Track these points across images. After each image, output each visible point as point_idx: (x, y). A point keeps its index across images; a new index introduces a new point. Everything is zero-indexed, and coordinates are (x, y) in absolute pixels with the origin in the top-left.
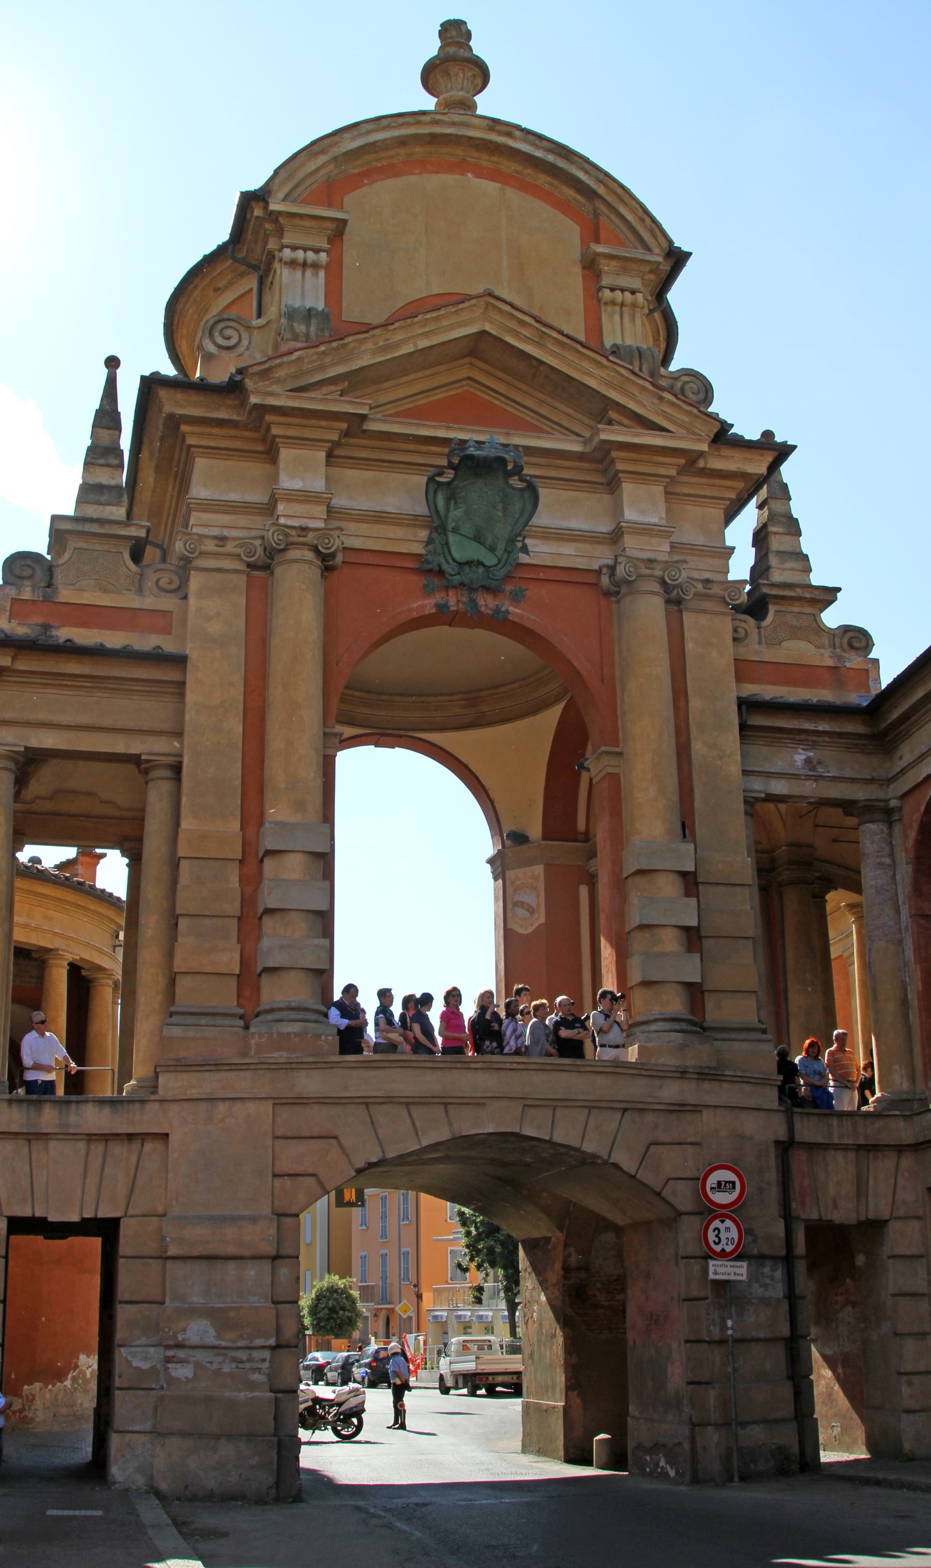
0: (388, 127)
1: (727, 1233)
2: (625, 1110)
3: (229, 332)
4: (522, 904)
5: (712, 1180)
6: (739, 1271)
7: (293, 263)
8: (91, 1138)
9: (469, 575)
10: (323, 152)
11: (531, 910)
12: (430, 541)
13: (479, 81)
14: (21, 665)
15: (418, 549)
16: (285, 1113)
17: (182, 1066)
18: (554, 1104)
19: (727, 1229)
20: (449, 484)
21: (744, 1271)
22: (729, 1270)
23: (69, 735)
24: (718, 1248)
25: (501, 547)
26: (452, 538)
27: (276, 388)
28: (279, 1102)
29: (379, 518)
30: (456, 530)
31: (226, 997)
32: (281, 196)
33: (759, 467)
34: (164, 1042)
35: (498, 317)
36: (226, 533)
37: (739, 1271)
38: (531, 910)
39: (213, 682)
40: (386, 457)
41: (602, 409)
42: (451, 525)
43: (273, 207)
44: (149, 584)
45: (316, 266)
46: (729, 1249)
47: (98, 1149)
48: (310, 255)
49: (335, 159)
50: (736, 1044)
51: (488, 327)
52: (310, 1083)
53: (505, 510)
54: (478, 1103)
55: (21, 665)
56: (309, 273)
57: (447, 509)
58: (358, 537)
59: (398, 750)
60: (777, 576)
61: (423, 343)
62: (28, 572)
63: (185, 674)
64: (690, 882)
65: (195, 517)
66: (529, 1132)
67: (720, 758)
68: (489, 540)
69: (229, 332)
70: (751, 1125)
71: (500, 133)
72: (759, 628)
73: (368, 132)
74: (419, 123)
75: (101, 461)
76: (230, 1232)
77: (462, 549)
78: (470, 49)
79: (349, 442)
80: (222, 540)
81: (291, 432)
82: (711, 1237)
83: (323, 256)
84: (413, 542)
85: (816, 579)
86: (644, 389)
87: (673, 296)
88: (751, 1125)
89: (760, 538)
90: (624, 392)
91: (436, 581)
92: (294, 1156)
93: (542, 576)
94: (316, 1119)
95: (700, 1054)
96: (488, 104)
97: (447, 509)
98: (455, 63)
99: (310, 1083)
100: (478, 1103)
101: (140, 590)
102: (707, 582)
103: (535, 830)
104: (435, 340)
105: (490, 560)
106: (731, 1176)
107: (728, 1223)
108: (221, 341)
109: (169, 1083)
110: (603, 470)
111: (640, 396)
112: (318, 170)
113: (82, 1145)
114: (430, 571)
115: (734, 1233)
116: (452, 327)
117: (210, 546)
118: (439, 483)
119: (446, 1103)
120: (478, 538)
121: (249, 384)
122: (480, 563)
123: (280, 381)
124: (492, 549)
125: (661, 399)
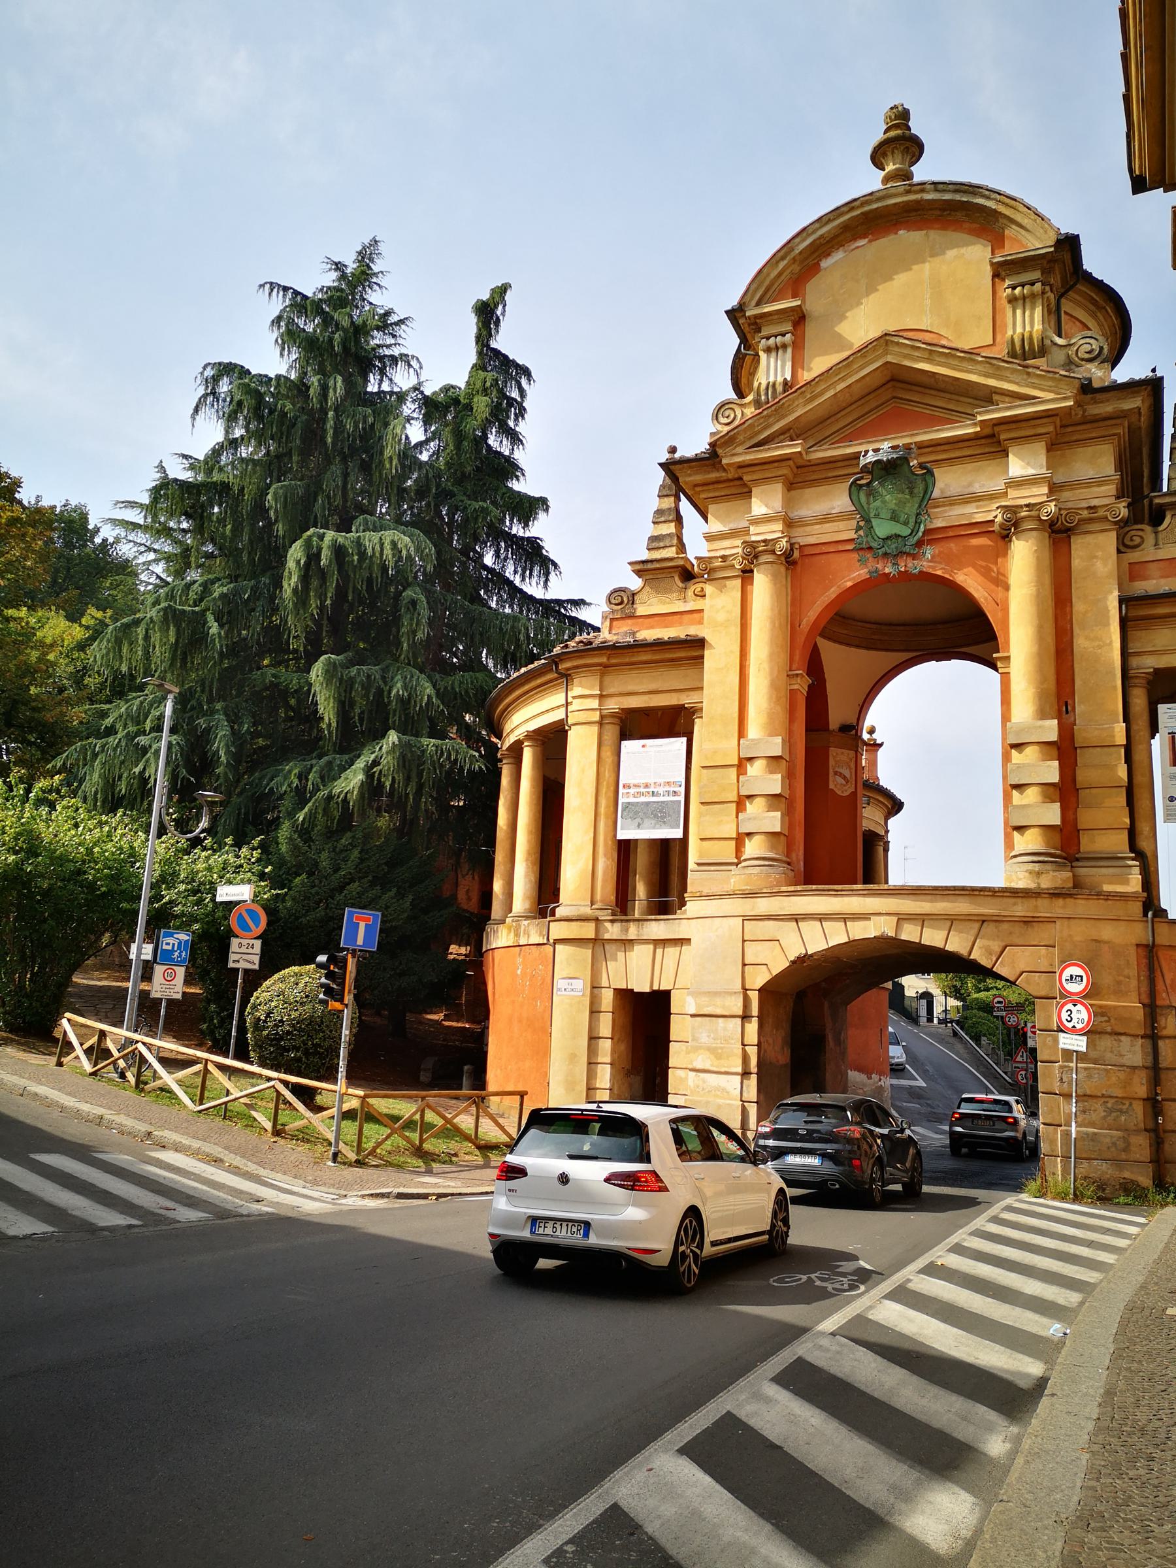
0: (829, 221)
2: (983, 921)
3: (727, 413)
4: (841, 775)
5: (1067, 974)
6: (1080, 1043)
7: (768, 350)
9: (892, 547)
10: (783, 259)
12: (858, 528)
13: (916, 150)
15: (852, 535)
19: (1079, 1011)
20: (868, 485)
21: (1084, 1044)
22: (1073, 1042)
23: (646, 697)
24: (1070, 1025)
25: (912, 520)
26: (875, 522)
27: (739, 450)
28: (747, 919)
29: (826, 519)
30: (877, 516)
31: (727, 851)
32: (754, 303)
35: (896, 349)
36: (727, 552)
37: (1080, 1043)
39: (719, 662)
40: (830, 474)
41: (988, 397)
42: (872, 515)
43: (748, 314)
45: (784, 346)
46: (1079, 1026)
49: (794, 259)
50: (1104, 871)
51: (890, 358)
52: (764, 905)
53: (911, 493)
54: (864, 917)
55: (613, 661)
56: (780, 352)
57: (868, 503)
58: (810, 536)
66: (926, 941)
67: (1100, 647)
68: (903, 518)
69: (727, 413)
70: (1108, 932)
71: (917, 192)
72: (1156, 533)
73: (814, 232)
74: (852, 209)
75: (663, 519)
76: (718, 1001)
77: (883, 529)
78: (909, 129)
79: (800, 476)
81: (755, 477)
82: (1064, 1016)
84: (845, 531)
86: (1015, 370)
88: (1108, 932)
90: (999, 378)
91: (869, 555)
93: (951, 534)
97: (868, 503)
98: (900, 143)
100: (864, 917)
102: (1091, 508)
105: (905, 531)
107: (1079, 1007)
108: (726, 421)
110: (993, 443)
111: (1012, 377)
112: (780, 274)
113: (651, 947)
114: (863, 548)
115: (1084, 1015)
116: (862, 368)
118: (861, 486)
119: (845, 918)
120: (894, 517)
122: (897, 536)
124: (906, 523)
125: (1028, 374)
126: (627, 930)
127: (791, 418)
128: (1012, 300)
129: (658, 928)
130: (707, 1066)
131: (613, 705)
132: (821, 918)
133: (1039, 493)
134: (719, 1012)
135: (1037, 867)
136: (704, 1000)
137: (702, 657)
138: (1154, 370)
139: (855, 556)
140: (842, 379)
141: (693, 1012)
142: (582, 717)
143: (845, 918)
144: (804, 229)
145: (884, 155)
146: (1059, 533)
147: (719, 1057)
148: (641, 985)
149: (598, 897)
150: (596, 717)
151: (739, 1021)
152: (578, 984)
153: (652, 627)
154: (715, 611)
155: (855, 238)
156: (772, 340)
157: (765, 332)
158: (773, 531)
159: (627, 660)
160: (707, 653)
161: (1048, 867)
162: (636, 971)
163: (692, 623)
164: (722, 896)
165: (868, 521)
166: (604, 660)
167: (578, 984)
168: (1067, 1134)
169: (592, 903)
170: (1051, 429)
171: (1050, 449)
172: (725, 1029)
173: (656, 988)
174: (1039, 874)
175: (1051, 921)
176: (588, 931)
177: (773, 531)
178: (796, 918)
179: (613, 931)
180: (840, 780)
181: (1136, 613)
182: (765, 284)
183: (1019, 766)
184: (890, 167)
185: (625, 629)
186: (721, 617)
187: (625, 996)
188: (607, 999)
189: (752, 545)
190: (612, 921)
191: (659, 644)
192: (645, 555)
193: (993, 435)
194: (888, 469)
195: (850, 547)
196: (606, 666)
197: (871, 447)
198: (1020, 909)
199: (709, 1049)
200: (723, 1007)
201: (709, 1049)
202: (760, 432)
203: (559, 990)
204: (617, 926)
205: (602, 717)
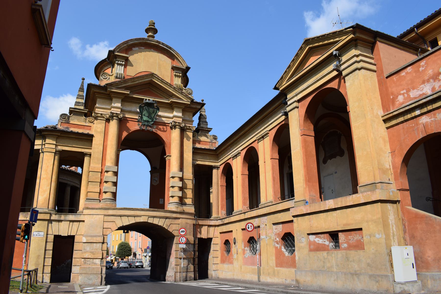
1: (184, 240)
4: (155, 180)
5: (181, 231)
7: (118, 64)
8: (71, 221)
10: (125, 44)
11: (157, 181)
14: (62, 135)
16: (106, 217)
17: (88, 208)
18: (154, 217)
26: (143, 116)
28: (105, 215)
30: (144, 115)
31: (96, 196)
33: (199, 107)
34: (85, 204)
38: (157, 181)
39: (97, 141)
41: (172, 96)
44: (87, 121)
47: (71, 223)
48: (121, 62)
52: (111, 212)
55: (62, 135)
59: (134, 151)
60: (202, 125)
61: (140, 81)
62: (64, 117)
63: (69, 185)
64: (181, 179)
65: (97, 110)
66: (149, 221)
80: (101, 114)
82: (180, 240)
83: (124, 63)
85: (209, 127)
87: (188, 74)
88: (189, 221)
89: (200, 118)
92: (106, 225)
94: (112, 218)
95: (180, 209)
96: (157, 37)
98: (152, 30)
99: (111, 212)
101: (85, 122)
103: (158, 167)
104: (142, 81)
106: (184, 230)
109: (86, 212)
110: (171, 107)
115: (185, 240)
117: (99, 115)
119: (135, 216)
121: (108, 87)
123: (114, 86)
126: (61, 217)
127: (127, 84)
128: (175, 75)
129: (71, 217)
130: (90, 257)
131: (60, 148)
132: (128, 216)
133: (180, 120)
134: (95, 241)
135: (177, 206)
136: (89, 238)
137: (92, 140)
138: (203, 101)
139: (137, 123)
140: (141, 80)
141: (85, 241)
142: (49, 150)
143: (135, 216)
144: (132, 40)
145: (149, 30)
146: (183, 130)
147: (94, 254)
148: (64, 233)
149: (50, 207)
150: (54, 151)
151: (101, 244)
152: (42, 233)
153: (75, 128)
154: (96, 128)
155: (142, 46)
156: (119, 62)
157: (289, 96)
158: (118, 111)
159: (67, 136)
160: (94, 138)
161: (179, 206)
162: (63, 229)
163: (87, 129)
164: (97, 209)
165: (142, 116)
166: (59, 134)
167: (42, 233)
168: (180, 267)
169: (48, 208)
170: (184, 107)
171: (122, 101)
172: (96, 246)
173: (69, 234)
174: (178, 207)
175: (179, 218)
176: (47, 217)
177: (118, 111)
178: (121, 216)
179: (54, 217)
180: (155, 181)
181: (196, 152)
182: (120, 48)
183: (107, 177)
184: (150, 34)
185: (66, 126)
186: (99, 130)
187: (57, 238)
188: (51, 238)
189: (113, 113)
190: (56, 214)
191: (78, 134)
192: (73, 106)
193: (109, 95)
194: (150, 105)
195: (137, 120)
196: (59, 136)
197: (148, 98)
198: (174, 215)
199: (91, 252)
200: (96, 240)
201: (91, 252)
202: (119, 85)
203: (33, 235)
204: (57, 215)
205: (56, 151)
